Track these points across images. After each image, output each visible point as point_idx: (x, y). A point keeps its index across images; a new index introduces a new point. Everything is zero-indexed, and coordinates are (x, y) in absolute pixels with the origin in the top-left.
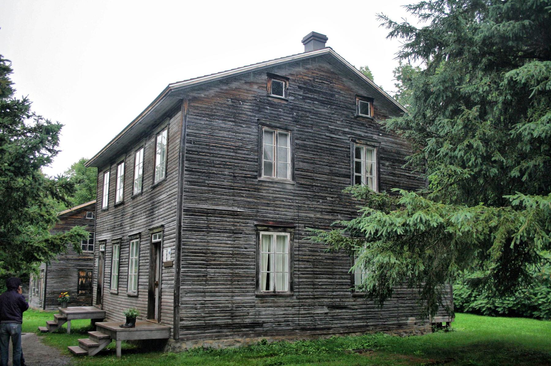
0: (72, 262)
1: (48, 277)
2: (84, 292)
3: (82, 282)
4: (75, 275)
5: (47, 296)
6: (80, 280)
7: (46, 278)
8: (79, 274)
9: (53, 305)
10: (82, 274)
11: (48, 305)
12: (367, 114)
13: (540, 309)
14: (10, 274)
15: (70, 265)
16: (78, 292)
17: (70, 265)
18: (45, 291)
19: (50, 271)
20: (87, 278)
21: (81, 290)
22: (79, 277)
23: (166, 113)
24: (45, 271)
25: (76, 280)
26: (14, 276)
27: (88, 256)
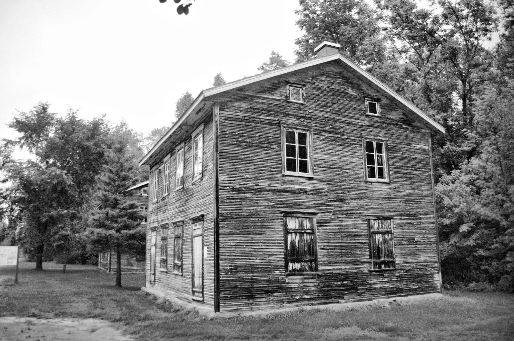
0: (269, 197)
1: (221, 231)
2: (298, 266)
3: (293, 243)
4: (278, 226)
5: (223, 277)
6: (290, 237)
7: (217, 235)
8: (285, 225)
9: (236, 298)
10: (293, 224)
11: (226, 298)
12: (376, 113)
13: (467, 252)
14: (110, 235)
15: (266, 204)
16: (286, 267)
17: (266, 204)
18: (217, 265)
19: (226, 218)
20: (301, 234)
21: (293, 261)
22: (287, 232)
23: (240, 89)
24: (211, 215)
25: (279, 236)
26: (117, 238)
27: (300, 184)
